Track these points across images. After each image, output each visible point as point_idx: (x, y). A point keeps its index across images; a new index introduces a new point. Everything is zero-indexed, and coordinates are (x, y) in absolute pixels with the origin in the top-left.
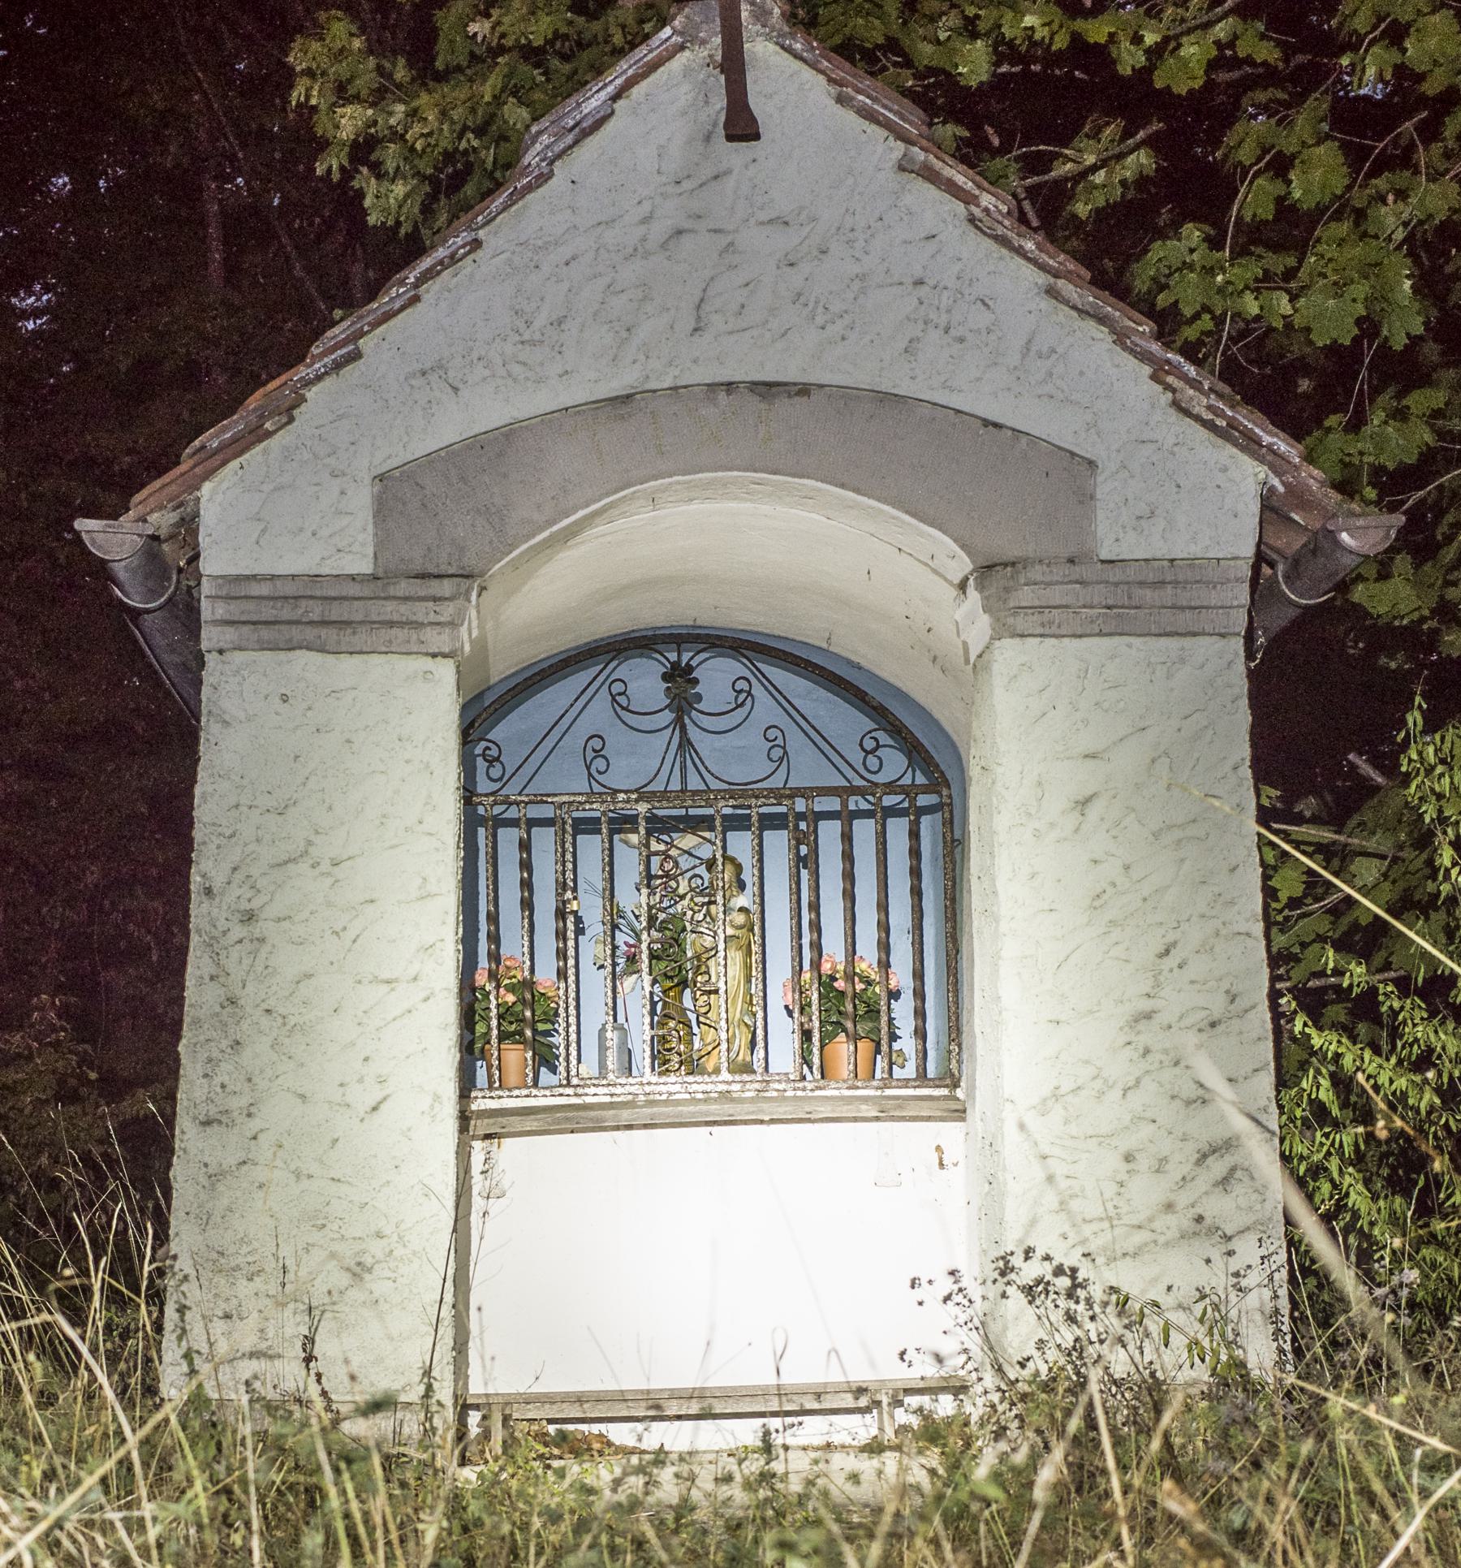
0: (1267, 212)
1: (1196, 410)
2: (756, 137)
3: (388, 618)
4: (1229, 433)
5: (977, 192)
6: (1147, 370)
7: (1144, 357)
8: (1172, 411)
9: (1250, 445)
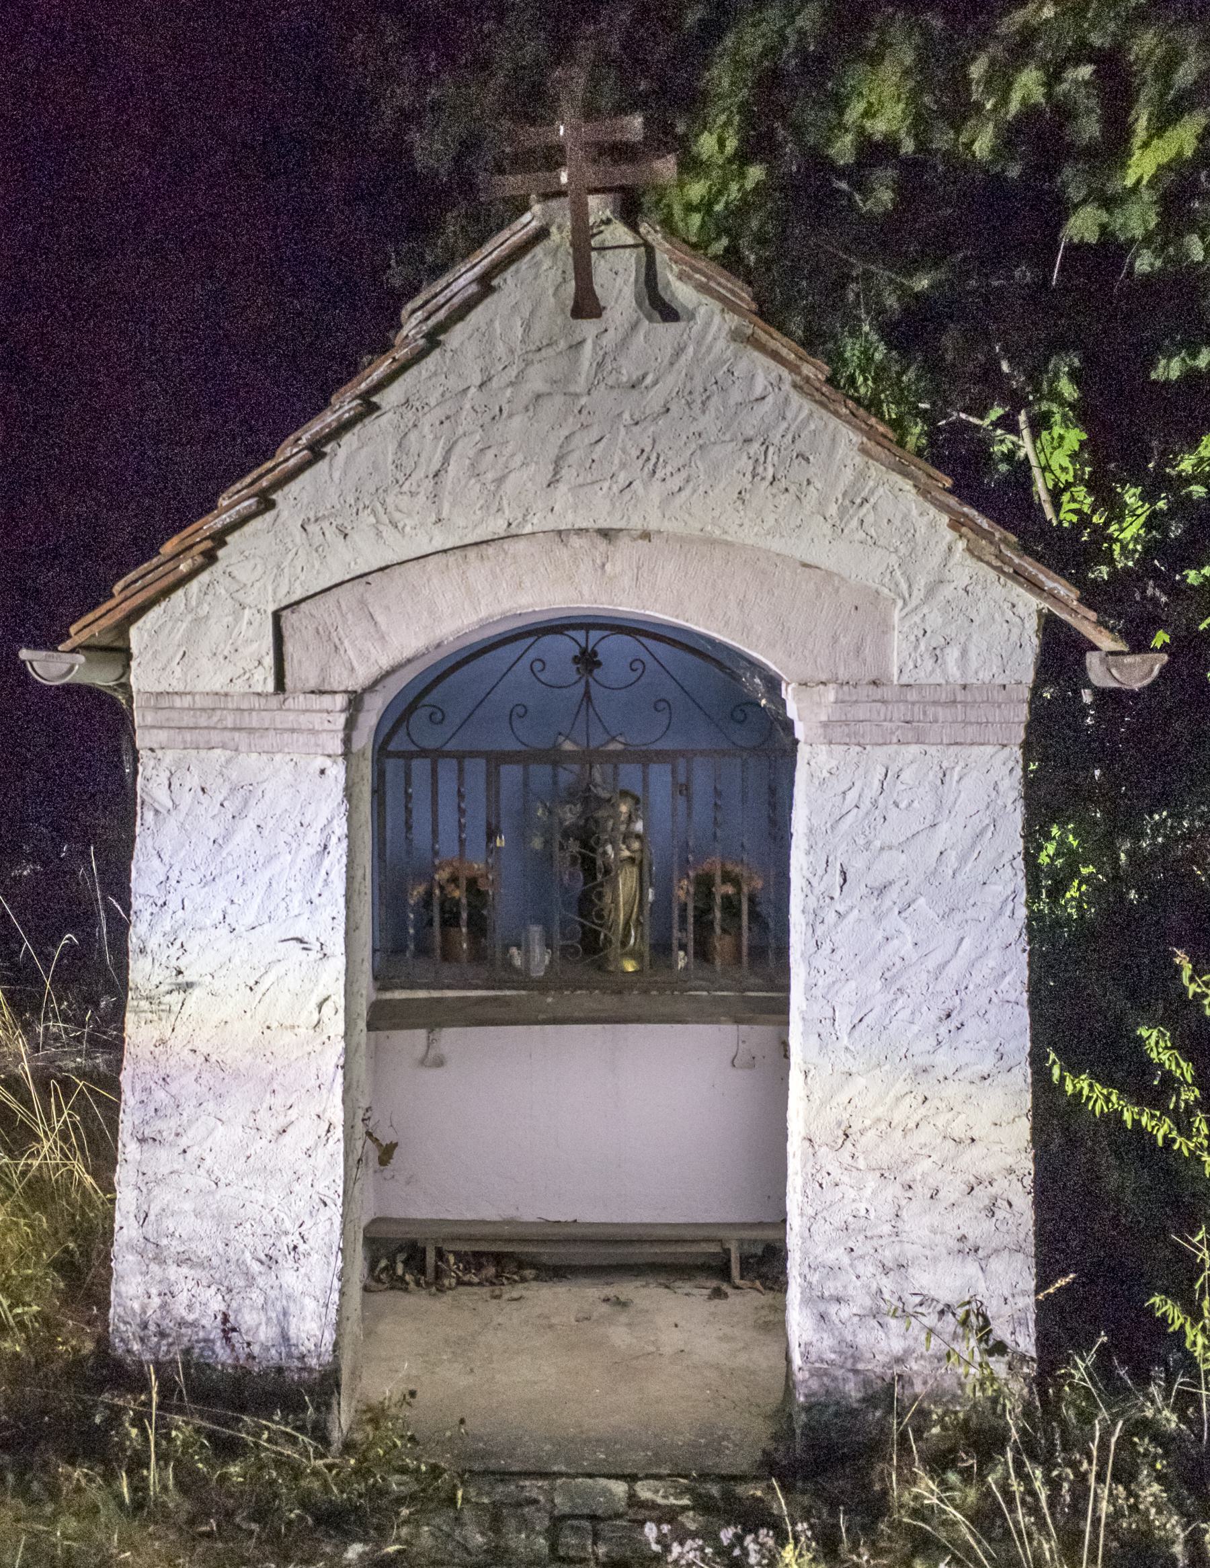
0: (1092, 237)
1: (987, 558)
2: (599, 315)
3: (289, 726)
4: (1017, 575)
5: (799, 363)
6: (945, 519)
7: (943, 508)
8: (967, 554)
9: (1035, 586)
